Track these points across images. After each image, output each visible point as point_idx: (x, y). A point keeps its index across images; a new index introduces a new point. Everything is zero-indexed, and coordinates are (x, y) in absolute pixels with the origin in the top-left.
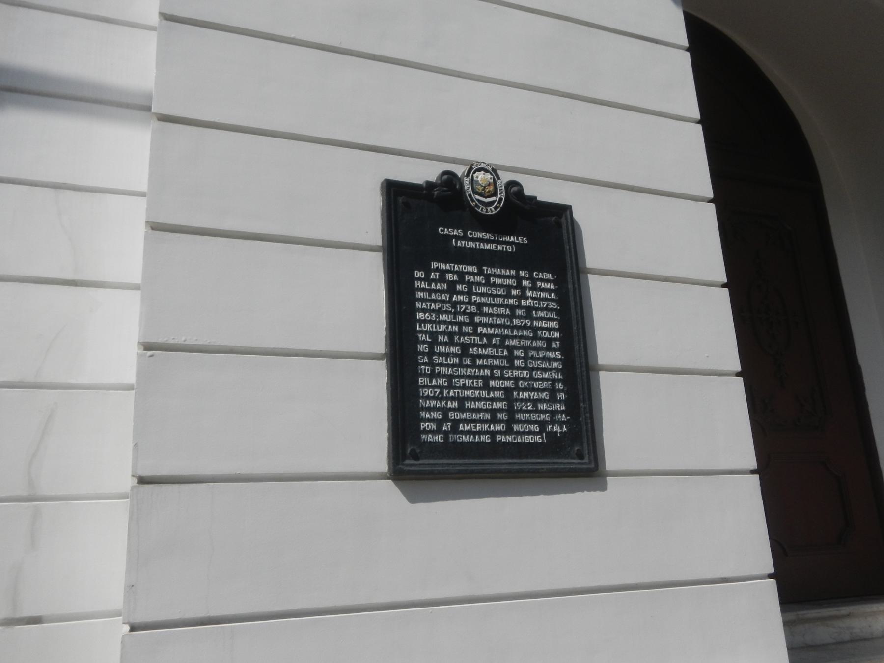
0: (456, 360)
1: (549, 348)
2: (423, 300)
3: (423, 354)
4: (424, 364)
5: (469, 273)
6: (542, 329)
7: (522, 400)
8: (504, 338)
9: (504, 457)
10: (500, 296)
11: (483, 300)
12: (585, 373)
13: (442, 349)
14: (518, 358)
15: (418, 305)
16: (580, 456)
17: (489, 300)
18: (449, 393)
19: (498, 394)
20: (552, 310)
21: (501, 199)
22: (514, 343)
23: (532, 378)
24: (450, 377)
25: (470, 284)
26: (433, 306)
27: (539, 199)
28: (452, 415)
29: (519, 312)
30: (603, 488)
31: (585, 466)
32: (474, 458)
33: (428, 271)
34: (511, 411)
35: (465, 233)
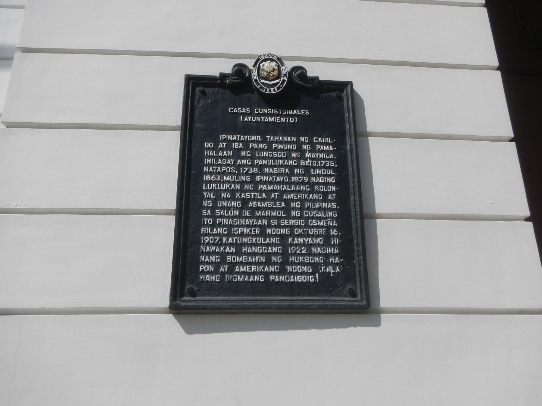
1: (325, 200)
3: (207, 208)
5: (253, 142)
14: (295, 209)
20: (329, 168)
22: (291, 196)
28: (229, 259)
34: (285, 254)
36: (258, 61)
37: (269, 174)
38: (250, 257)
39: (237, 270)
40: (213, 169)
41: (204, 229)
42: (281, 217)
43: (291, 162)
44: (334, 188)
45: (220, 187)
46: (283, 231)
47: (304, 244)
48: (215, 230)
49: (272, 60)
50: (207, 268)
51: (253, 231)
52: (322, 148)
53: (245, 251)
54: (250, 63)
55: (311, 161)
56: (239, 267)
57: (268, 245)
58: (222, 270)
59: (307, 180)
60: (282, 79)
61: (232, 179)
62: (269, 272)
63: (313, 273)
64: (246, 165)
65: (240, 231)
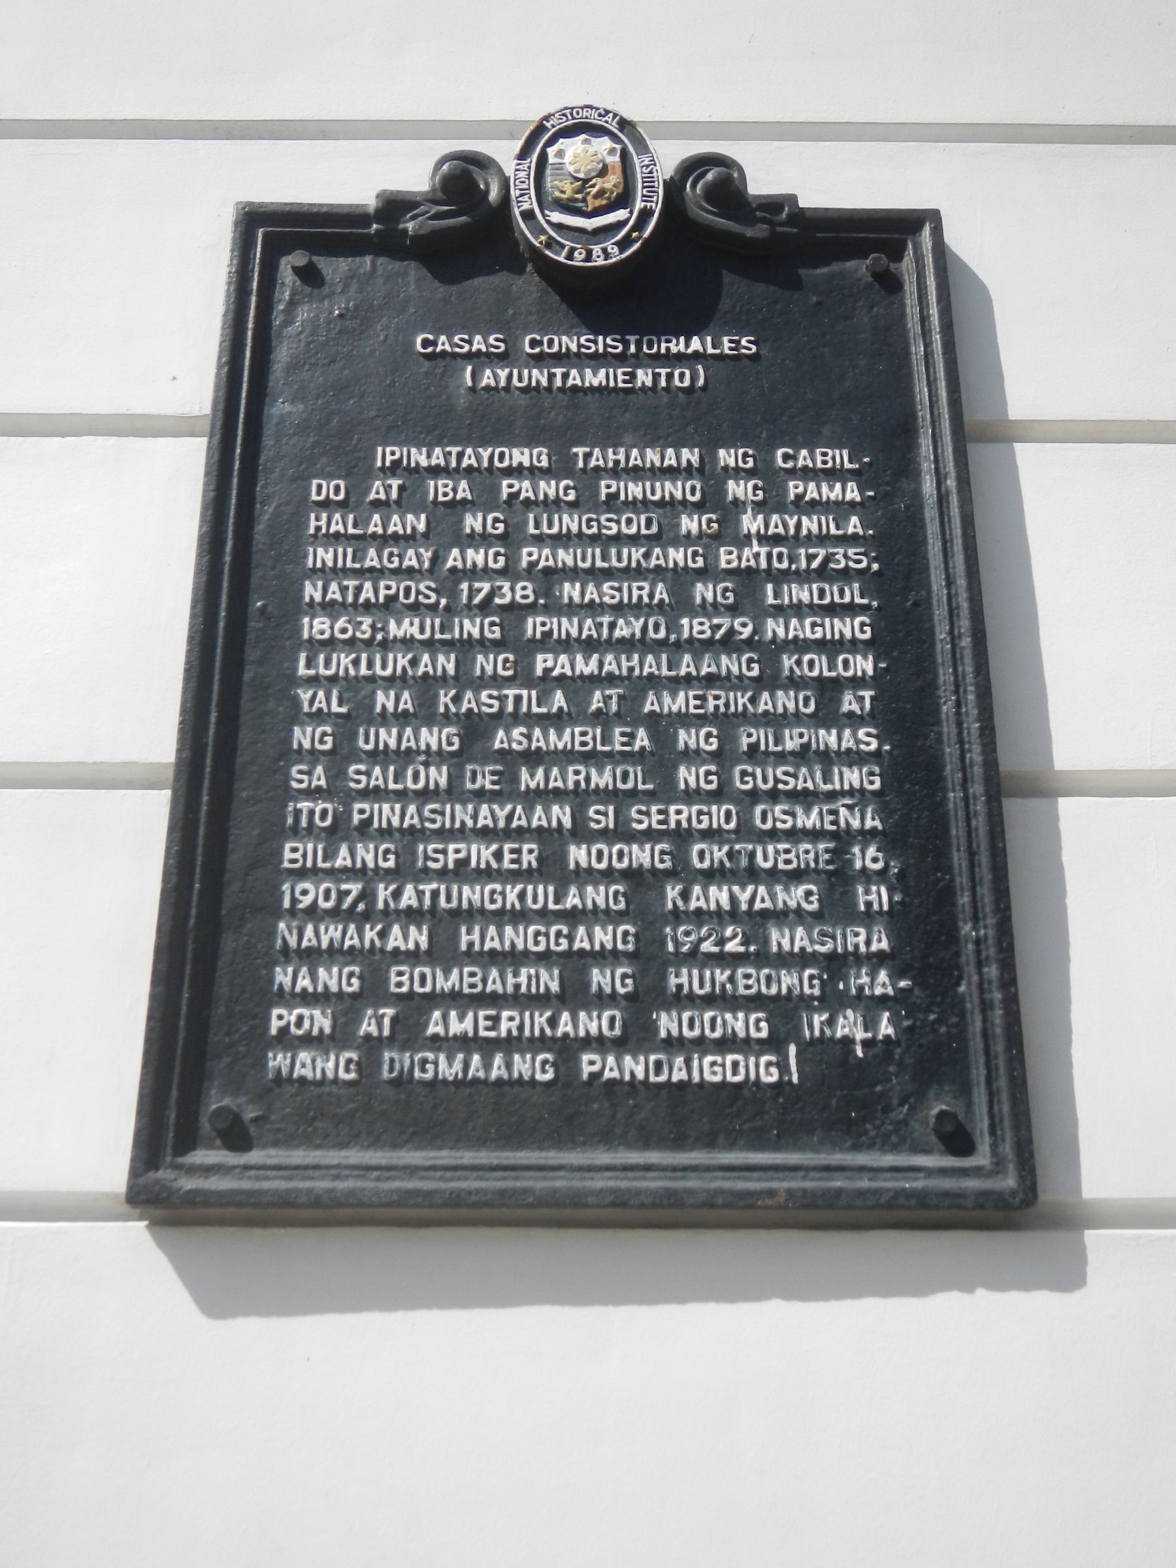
0: (439, 776)
1: (827, 716)
4: (313, 793)
6: (799, 646)
9: (606, 1139)
10: (635, 540)
11: (565, 557)
12: (980, 807)
13: (388, 737)
14: (692, 756)
16: (957, 1140)
17: (593, 557)
18: (397, 895)
19: (597, 896)
20: (846, 575)
21: (646, 214)
22: (677, 702)
23: (746, 831)
26: (367, 593)
27: (806, 202)
28: (400, 979)
29: (703, 591)
30: (1069, 1275)
31: (972, 1184)
32: (482, 1142)
33: (358, 472)
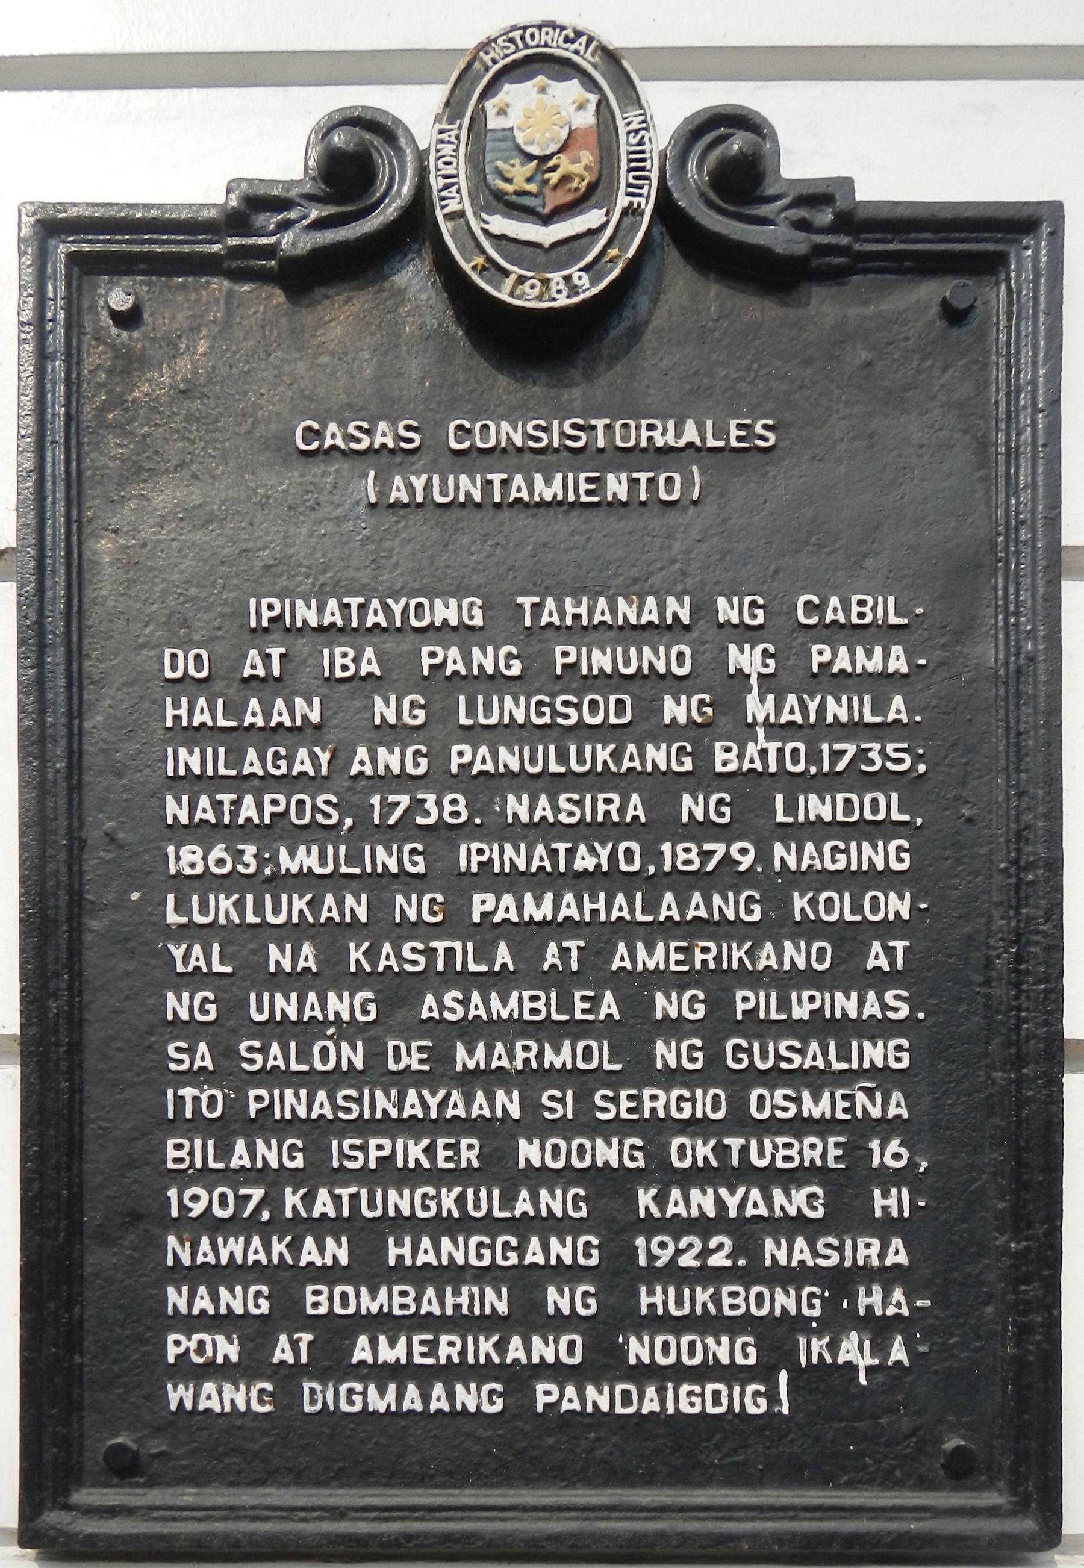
1: (849, 974)
2: (195, 784)
3: (190, 1030)
5: (441, 632)
7: (678, 1227)
8: (602, 936)
14: (675, 1028)
15: (176, 810)
20: (882, 780)
22: (655, 958)
24: (316, 1133)
25: (440, 685)
28: (317, 1300)
34: (619, 1275)
35: (431, 429)
36: (475, 80)
37: (531, 825)
38: (430, 1292)
39: (361, 1353)
40: (217, 805)
41: (179, 1147)
42: (601, 1077)
43: (657, 755)
44: (898, 906)
45: (259, 909)
46: (607, 1153)
47: (720, 1223)
48: (240, 1147)
49: (560, 67)
50: (201, 1344)
51: (441, 1154)
52: (842, 662)
53: (400, 1258)
54: (417, 108)
55: (773, 747)
56: (374, 1343)
57: (523, 1226)
58: (283, 1353)
59: (746, 862)
60: (623, 201)
61: (323, 862)
62: (530, 1365)
63: (764, 1372)
64: (403, 781)
65: (373, 1154)
